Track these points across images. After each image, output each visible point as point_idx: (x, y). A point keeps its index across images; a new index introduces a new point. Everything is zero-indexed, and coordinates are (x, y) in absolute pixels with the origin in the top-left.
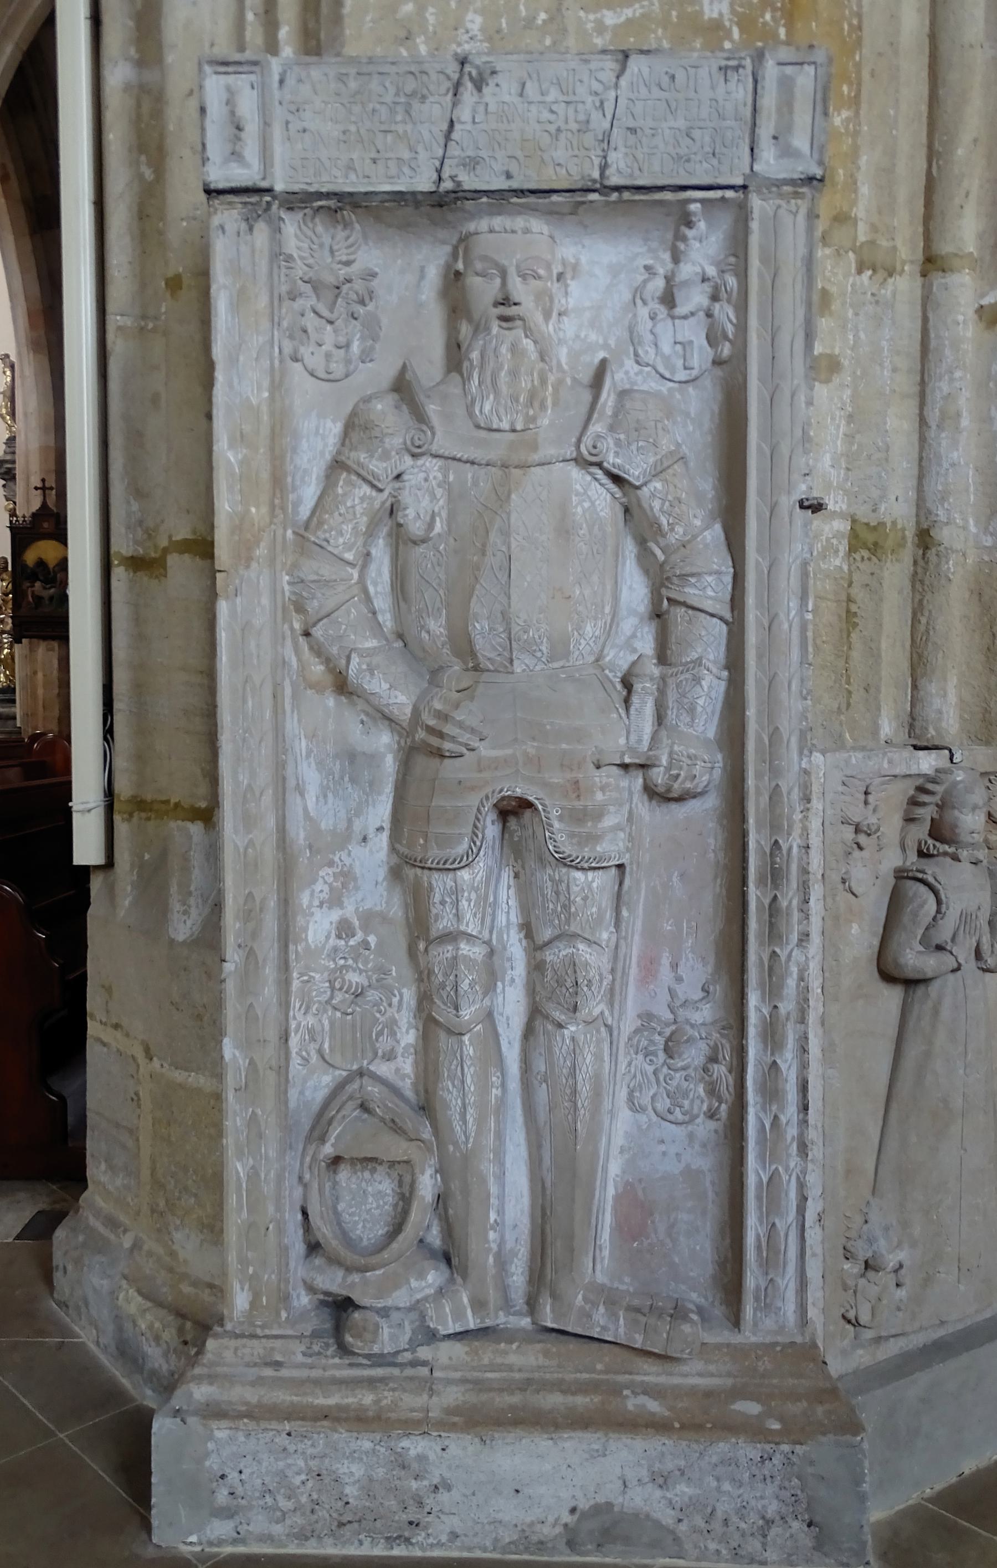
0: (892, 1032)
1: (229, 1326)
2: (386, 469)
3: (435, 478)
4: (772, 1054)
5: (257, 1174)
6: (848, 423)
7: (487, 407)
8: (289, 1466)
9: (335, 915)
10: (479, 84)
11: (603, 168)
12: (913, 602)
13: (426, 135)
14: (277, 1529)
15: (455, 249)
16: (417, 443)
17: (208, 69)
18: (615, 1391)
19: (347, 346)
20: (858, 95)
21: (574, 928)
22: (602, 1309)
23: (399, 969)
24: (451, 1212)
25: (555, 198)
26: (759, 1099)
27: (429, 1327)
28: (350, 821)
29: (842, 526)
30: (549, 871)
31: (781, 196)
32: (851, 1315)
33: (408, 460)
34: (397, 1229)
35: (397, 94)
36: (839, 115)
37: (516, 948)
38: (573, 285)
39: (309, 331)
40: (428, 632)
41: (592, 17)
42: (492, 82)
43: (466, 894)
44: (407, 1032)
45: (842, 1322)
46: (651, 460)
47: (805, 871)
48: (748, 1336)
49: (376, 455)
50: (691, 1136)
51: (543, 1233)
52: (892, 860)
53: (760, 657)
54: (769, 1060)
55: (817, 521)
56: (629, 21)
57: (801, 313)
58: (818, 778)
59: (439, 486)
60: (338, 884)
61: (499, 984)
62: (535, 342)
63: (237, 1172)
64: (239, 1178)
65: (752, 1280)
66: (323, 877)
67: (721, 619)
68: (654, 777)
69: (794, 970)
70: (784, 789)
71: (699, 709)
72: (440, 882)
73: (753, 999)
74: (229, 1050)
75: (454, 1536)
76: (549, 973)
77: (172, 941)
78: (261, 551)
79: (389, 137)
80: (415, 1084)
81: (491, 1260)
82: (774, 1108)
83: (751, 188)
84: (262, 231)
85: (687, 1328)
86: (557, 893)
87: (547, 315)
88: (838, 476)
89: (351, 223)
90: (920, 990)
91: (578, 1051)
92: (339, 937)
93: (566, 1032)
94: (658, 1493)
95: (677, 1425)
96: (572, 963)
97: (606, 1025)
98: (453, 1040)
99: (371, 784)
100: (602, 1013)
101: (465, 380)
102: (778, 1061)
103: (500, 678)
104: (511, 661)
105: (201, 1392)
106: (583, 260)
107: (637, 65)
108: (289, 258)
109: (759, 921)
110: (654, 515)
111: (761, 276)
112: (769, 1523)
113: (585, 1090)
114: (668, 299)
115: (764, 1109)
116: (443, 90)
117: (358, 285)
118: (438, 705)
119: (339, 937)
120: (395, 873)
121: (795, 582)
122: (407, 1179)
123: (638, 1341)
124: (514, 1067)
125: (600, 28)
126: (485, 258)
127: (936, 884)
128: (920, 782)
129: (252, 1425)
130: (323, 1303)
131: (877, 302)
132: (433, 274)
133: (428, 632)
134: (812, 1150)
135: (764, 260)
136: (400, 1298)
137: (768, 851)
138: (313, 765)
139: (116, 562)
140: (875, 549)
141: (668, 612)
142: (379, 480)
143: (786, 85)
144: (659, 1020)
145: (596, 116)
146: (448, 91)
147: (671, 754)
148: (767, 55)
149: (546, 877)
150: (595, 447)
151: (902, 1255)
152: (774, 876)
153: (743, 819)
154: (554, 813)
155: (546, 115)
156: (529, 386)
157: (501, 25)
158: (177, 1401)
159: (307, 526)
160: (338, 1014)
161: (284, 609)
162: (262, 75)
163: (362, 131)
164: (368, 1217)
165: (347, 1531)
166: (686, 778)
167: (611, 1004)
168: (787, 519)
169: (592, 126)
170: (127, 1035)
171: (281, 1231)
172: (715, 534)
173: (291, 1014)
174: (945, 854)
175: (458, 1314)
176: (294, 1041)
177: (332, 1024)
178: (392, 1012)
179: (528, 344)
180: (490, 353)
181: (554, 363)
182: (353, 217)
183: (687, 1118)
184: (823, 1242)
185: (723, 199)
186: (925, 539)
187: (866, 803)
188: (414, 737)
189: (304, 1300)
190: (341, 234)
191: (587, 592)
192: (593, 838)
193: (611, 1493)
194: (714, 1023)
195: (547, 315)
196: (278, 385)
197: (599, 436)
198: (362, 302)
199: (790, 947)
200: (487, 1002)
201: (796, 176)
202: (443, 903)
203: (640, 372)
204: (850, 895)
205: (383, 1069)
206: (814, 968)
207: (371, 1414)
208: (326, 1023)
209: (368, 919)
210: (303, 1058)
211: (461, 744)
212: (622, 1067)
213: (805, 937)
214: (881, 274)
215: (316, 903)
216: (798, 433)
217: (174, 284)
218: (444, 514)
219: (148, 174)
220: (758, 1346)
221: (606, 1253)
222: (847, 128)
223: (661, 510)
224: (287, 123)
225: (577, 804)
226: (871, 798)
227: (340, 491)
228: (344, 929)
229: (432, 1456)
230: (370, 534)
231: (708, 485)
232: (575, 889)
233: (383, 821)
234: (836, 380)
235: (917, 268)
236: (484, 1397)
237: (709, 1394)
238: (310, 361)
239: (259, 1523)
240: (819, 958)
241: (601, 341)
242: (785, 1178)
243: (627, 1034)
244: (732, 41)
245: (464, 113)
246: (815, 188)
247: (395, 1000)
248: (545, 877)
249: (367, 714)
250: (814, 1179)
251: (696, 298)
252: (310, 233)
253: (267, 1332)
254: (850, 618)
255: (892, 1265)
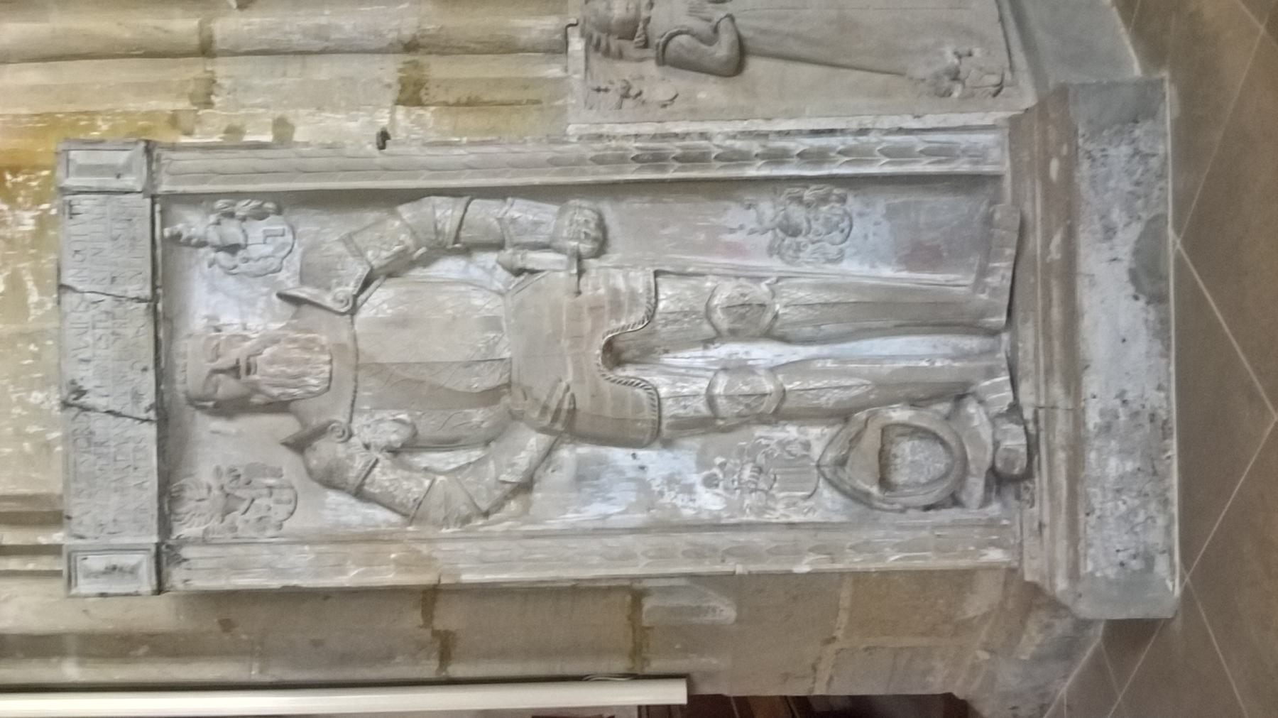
0: (780, 64)
1: (1015, 564)
2: (362, 456)
3: (367, 419)
4: (792, 157)
5: (897, 545)
6: (324, 110)
7: (314, 382)
8: (1112, 514)
9: (700, 489)
10: (81, 393)
11: (139, 300)
12: (458, 54)
13: (117, 431)
14: (1161, 521)
15: (199, 408)
16: (341, 433)
17: (74, 591)
18: (1048, 268)
19: (270, 487)
20: (86, 113)
21: (702, 308)
22: (989, 280)
23: (740, 439)
24: (922, 395)
25: (161, 335)
26: (827, 165)
27: (1007, 411)
28: (630, 480)
29: (401, 111)
30: (659, 328)
31: (158, 171)
32: (993, 90)
33: (353, 440)
34: (936, 438)
35: (89, 452)
36: (100, 126)
37: (722, 351)
38: (224, 320)
39: (259, 516)
40: (483, 422)
41: (32, 311)
42: (80, 383)
43: (678, 390)
44: (788, 432)
45: (999, 97)
46: (350, 259)
47: (654, 137)
48: (1006, 168)
49: (351, 464)
50: (861, 215)
51: (934, 325)
52: (651, 68)
53: (495, 175)
54: (796, 160)
55: (398, 135)
56: (37, 283)
57: (244, 153)
58: (586, 129)
59: (372, 416)
60: (677, 488)
61: (750, 363)
62: (265, 347)
63: (896, 560)
64: (901, 559)
65: (963, 167)
66: (672, 499)
67: (468, 204)
68: (586, 251)
69: (729, 143)
70: (593, 154)
71: (536, 219)
72: (670, 409)
73: (751, 172)
74: (803, 568)
75: (1160, 388)
76: (737, 326)
77: (738, 621)
78: (424, 549)
79: (119, 458)
80: (829, 426)
81: (957, 364)
82: (832, 154)
83: (153, 193)
84: (186, 552)
85: (997, 216)
86: (675, 321)
87: (246, 338)
88: (362, 116)
89: (181, 485)
90: (749, 44)
91: (795, 303)
92: (717, 486)
93: (780, 312)
94: (1120, 235)
95: (1069, 222)
96: (728, 309)
97: (777, 281)
98: (791, 398)
99: (600, 464)
100: (768, 285)
101: (294, 399)
102: (798, 152)
103: (515, 368)
104: (502, 360)
105: (1061, 584)
106: (205, 313)
107: (68, 280)
108: (206, 531)
109: (692, 169)
110: (392, 256)
111: (215, 183)
112: (1137, 152)
113: (826, 296)
114: (233, 249)
115: (834, 162)
116: (85, 419)
117: (225, 480)
118: (535, 414)
119: (717, 486)
120: (668, 444)
121: (440, 151)
122: (899, 430)
123: (1010, 251)
124: (812, 350)
125: (40, 305)
126: (205, 387)
127: (667, 35)
128: (591, 48)
129: (1082, 545)
130: (998, 492)
131: (235, 90)
132: (218, 424)
133: (483, 422)
134: (865, 125)
135: (204, 181)
136: (986, 434)
137: (639, 165)
138: (587, 508)
139: (444, 674)
140: (419, 84)
141: (464, 243)
142: (369, 462)
143: (84, 170)
144: (773, 241)
145: (103, 306)
146: (86, 415)
147: (572, 239)
148: (62, 185)
149: (664, 330)
150: (342, 301)
151: (948, 52)
152: (657, 159)
153: (615, 184)
154: (614, 324)
155: (102, 344)
156: (297, 351)
157: (38, 378)
158: (1068, 601)
159: (405, 515)
160: (776, 485)
161: (468, 531)
162: (78, 551)
163: (115, 477)
164: (931, 460)
165: (1160, 468)
166: (587, 228)
167: (761, 279)
168: (394, 158)
169: (109, 309)
170: (820, 658)
171: (940, 526)
172: (406, 211)
173: (774, 521)
174: (644, 28)
175: (996, 388)
176: (795, 518)
177: (782, 490)
178: (773, 443)
179: (267, 352)
180: (275, 380)
181: (281, 332)
182: (175, 485)
183: (847, 219)
184: (935, 114)
185: (162, 212)
186: (410, 46)
187: (606, 90)
188: (562, 432)
189: (995, 509)
190: (188, 494)
191: (450, 304)
192: (633, 295)
193: (1122, 270)
194: (773, 200)
195: (246, 338)
196: (301, 540)
197: (335, 299)
198: (238, 476)
199: (712, 146)
200: (762, 372)
201: (145, 161)
202: (685, 407)
203: (287, 267)
204: (676, 100)
205: (816, 451)
206: (729, 128)
207: (1071, 453)
208: (782, 494)
209: (702, 464)
210: (809, 511)
211: (564, 397)
212: (808, 268)
213: (703, 135)
214: (216, 90)
215: (691, 504)
216: (329, 152)
217: (227, 625)
218: (394, 412)
219: (143, 650)
220: (1012, 160)
221: (952, 276)
222: (110, 120)
223: (388, 250)
224: (110, 533)
225: (607, 307)
226: (603, 87)
227: (377, 491)
228: (710, 482)
229: (1100, 406)
230: (409, 468)
231: (371, 216)
232: (672, 308)
233: (628, 454)
234: (291, 120)
235: (209, 61)
236: (1056, 367)
237: (1046, 197)
238: (282, 515)
239: (1155, 537)
240: (720, 124)
241: (264, 298)
242: (884, 145)
243: (784, 265)
244: (50, 209)
245: (101, 403)
246: (154, 147)
247: (764, 442)
248: (664, 331)
249: (547, 467)
250: (887, 122)
251: (232, 231)
252: (187, 517)
253: (1018, 534)
254: (471, 103)
255: (956, 61)
